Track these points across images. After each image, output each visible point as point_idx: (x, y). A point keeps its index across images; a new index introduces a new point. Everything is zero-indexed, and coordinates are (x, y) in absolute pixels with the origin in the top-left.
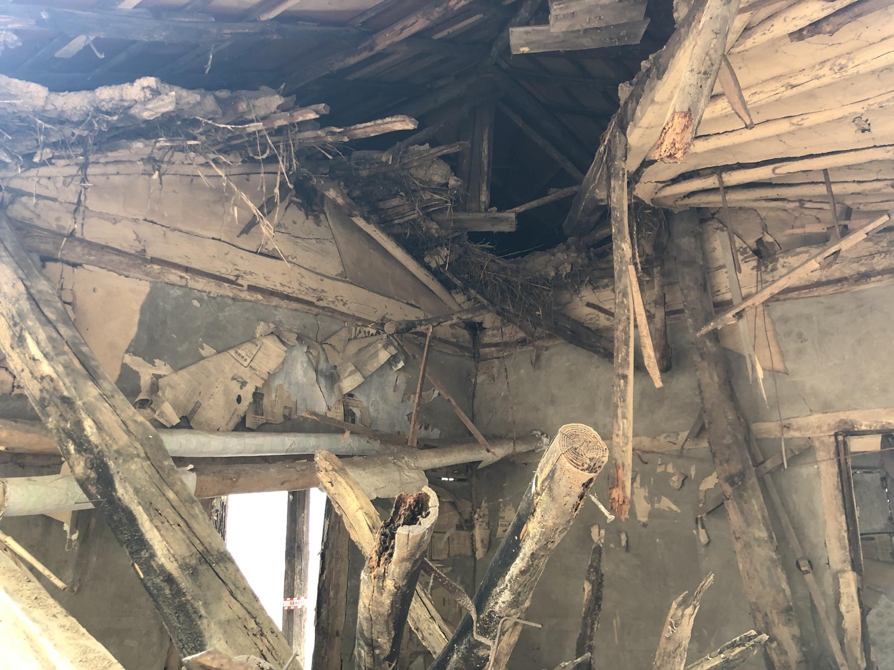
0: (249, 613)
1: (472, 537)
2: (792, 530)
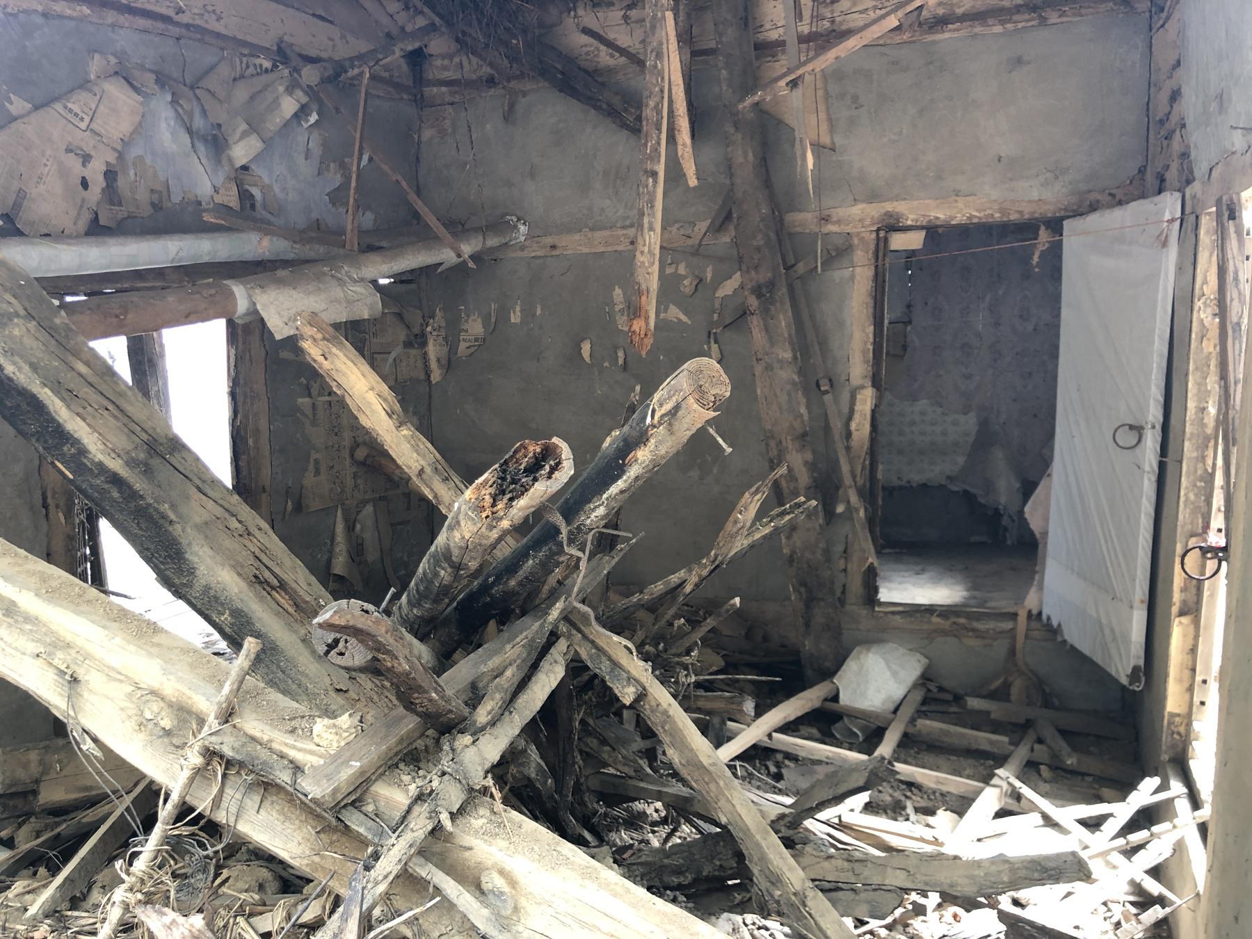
0: (227, 510)
1: (425, 356)
2: (817, 348)
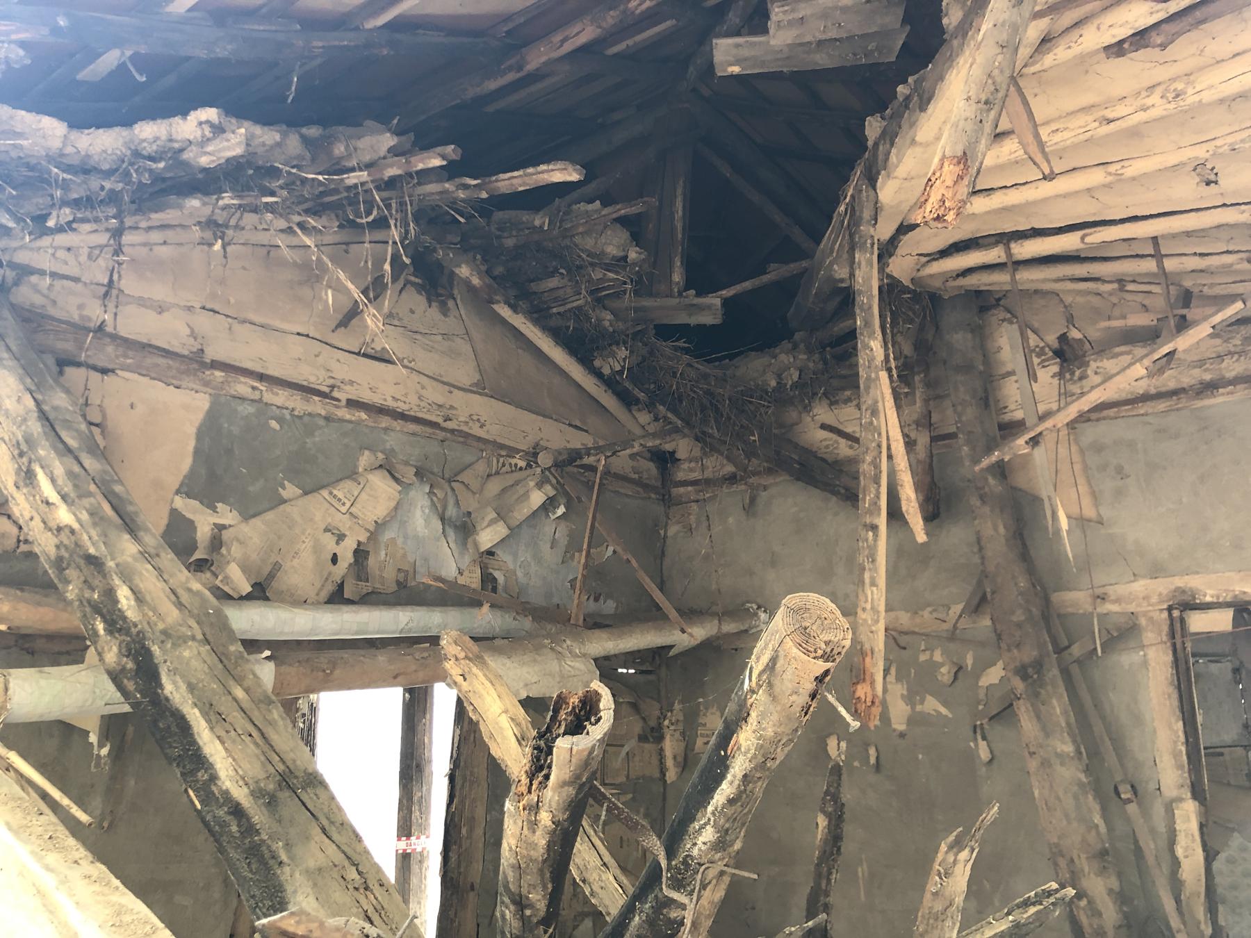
0: (348, 858)
1: (661, 752)
2: (1108, 743)
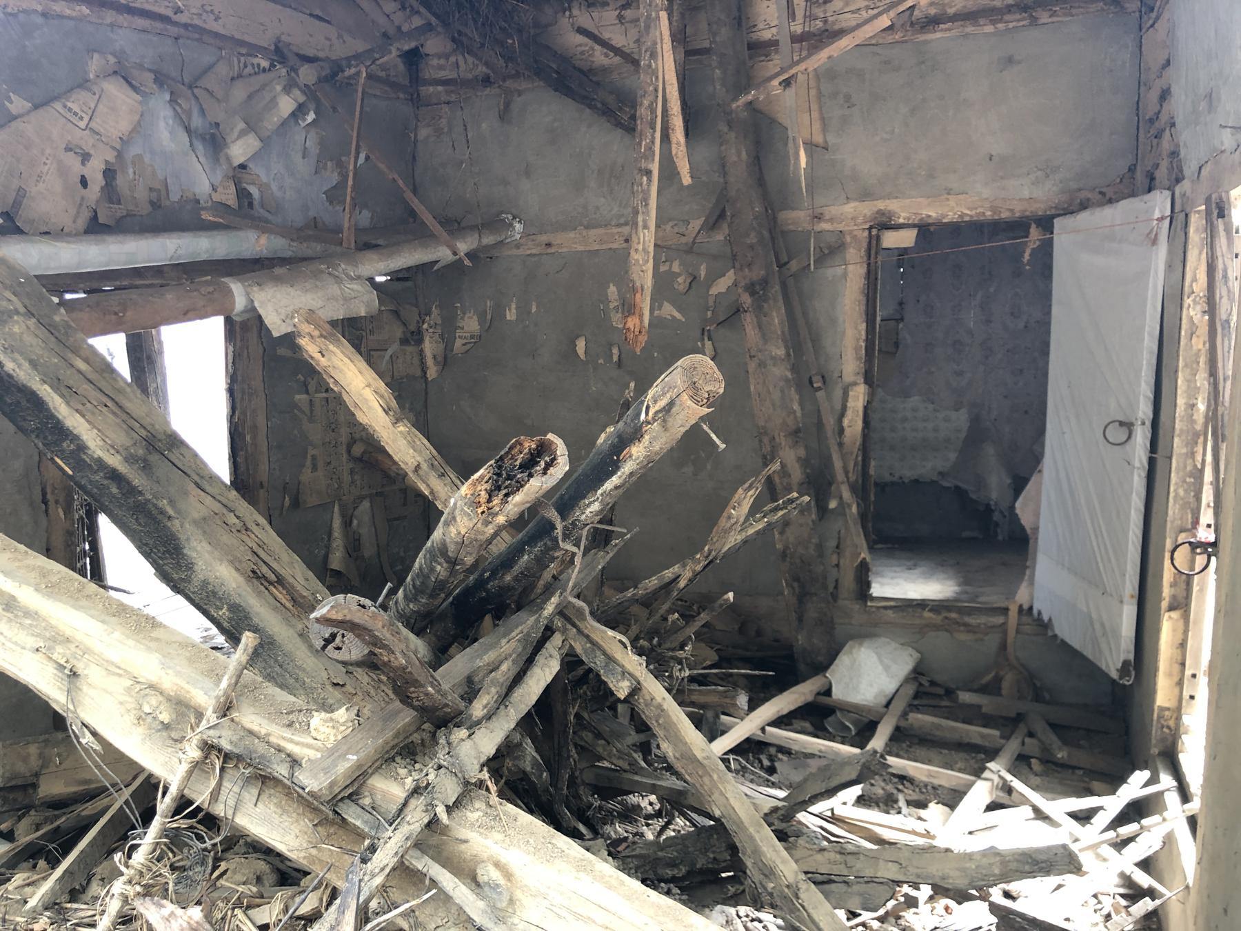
0: (225, 506)
1: (421, 353)
2: (810, 345)
